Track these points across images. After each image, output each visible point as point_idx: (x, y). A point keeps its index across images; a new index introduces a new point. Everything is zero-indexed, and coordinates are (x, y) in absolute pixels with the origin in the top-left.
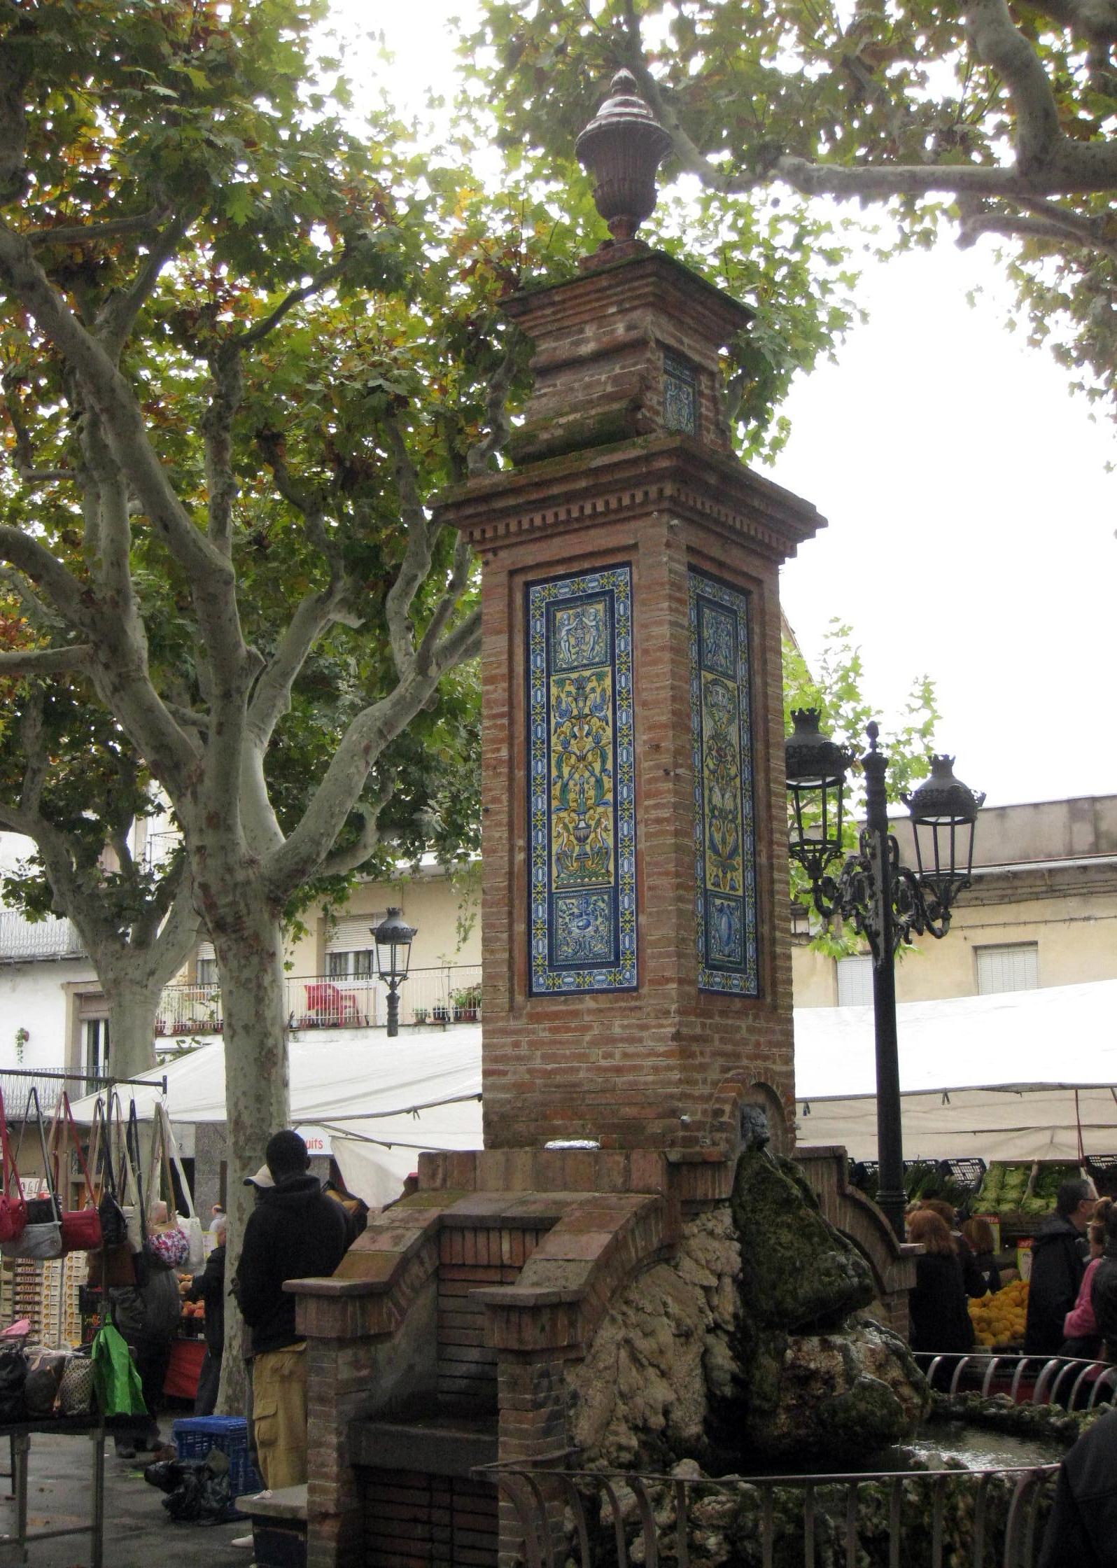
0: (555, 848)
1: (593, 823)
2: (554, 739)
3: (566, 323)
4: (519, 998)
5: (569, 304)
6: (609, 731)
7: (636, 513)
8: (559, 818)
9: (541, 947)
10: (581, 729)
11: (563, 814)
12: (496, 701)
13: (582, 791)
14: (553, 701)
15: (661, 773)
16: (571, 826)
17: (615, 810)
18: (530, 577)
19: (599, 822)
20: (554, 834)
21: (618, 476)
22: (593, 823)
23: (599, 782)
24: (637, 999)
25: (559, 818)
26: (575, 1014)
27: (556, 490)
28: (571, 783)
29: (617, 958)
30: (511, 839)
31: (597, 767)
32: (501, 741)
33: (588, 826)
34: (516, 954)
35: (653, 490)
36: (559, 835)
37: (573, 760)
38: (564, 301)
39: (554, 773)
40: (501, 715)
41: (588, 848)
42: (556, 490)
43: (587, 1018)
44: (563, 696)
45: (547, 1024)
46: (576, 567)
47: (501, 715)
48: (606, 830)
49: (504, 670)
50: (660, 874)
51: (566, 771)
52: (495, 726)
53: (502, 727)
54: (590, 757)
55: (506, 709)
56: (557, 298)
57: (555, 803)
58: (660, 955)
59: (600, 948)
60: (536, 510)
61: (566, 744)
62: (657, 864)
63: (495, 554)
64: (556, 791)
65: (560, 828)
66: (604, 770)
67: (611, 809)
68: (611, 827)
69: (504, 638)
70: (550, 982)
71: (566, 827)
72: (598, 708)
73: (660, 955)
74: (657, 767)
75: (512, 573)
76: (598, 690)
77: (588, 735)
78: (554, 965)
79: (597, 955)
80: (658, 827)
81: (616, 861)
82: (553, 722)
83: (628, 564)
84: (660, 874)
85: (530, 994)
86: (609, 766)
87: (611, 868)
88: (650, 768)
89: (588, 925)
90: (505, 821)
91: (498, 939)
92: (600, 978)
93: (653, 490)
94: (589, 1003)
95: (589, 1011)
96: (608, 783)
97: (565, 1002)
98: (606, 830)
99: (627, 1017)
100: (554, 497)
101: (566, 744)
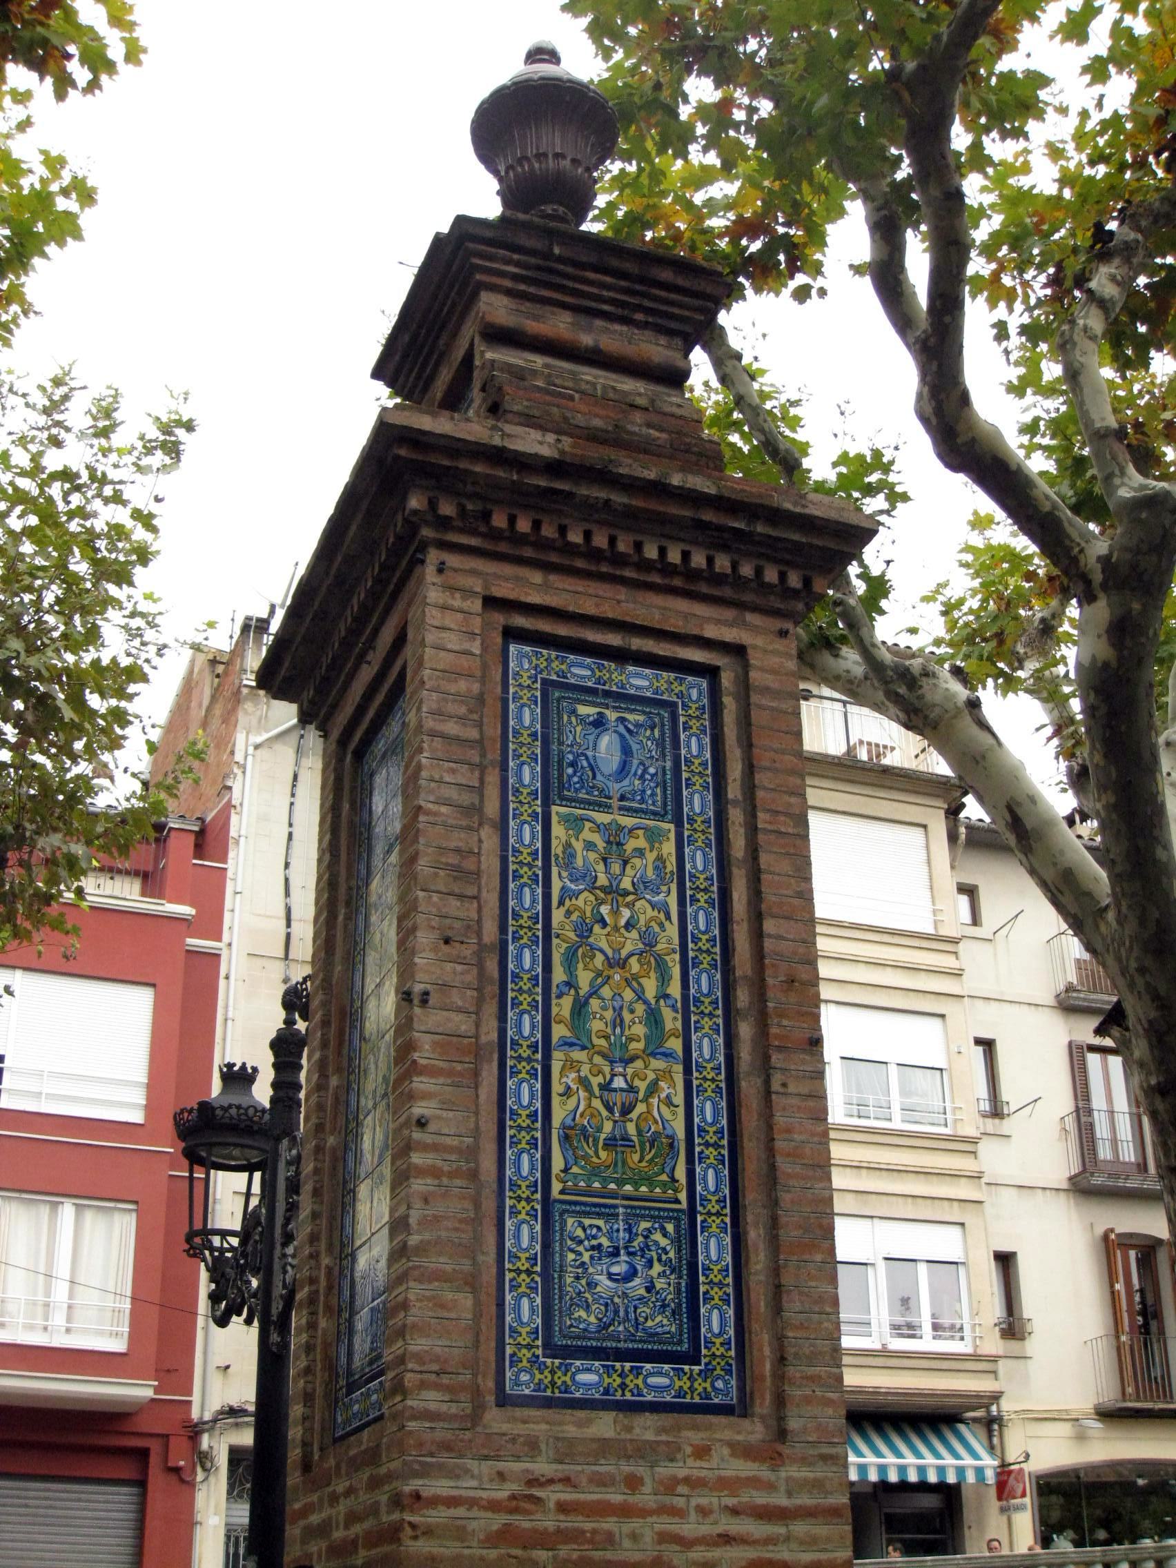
2: (557, 916)
13: (618, 1022)
18: (520, 621)
23: (653, 1017)
25: (571, 1065)
31: (650, 987)
39: (559, 975)
61: (584, 931)
64: (563, 1007)
86: (675, 989)
92: (658, 1380)
96: (671, 1020)
101: (584, 931)
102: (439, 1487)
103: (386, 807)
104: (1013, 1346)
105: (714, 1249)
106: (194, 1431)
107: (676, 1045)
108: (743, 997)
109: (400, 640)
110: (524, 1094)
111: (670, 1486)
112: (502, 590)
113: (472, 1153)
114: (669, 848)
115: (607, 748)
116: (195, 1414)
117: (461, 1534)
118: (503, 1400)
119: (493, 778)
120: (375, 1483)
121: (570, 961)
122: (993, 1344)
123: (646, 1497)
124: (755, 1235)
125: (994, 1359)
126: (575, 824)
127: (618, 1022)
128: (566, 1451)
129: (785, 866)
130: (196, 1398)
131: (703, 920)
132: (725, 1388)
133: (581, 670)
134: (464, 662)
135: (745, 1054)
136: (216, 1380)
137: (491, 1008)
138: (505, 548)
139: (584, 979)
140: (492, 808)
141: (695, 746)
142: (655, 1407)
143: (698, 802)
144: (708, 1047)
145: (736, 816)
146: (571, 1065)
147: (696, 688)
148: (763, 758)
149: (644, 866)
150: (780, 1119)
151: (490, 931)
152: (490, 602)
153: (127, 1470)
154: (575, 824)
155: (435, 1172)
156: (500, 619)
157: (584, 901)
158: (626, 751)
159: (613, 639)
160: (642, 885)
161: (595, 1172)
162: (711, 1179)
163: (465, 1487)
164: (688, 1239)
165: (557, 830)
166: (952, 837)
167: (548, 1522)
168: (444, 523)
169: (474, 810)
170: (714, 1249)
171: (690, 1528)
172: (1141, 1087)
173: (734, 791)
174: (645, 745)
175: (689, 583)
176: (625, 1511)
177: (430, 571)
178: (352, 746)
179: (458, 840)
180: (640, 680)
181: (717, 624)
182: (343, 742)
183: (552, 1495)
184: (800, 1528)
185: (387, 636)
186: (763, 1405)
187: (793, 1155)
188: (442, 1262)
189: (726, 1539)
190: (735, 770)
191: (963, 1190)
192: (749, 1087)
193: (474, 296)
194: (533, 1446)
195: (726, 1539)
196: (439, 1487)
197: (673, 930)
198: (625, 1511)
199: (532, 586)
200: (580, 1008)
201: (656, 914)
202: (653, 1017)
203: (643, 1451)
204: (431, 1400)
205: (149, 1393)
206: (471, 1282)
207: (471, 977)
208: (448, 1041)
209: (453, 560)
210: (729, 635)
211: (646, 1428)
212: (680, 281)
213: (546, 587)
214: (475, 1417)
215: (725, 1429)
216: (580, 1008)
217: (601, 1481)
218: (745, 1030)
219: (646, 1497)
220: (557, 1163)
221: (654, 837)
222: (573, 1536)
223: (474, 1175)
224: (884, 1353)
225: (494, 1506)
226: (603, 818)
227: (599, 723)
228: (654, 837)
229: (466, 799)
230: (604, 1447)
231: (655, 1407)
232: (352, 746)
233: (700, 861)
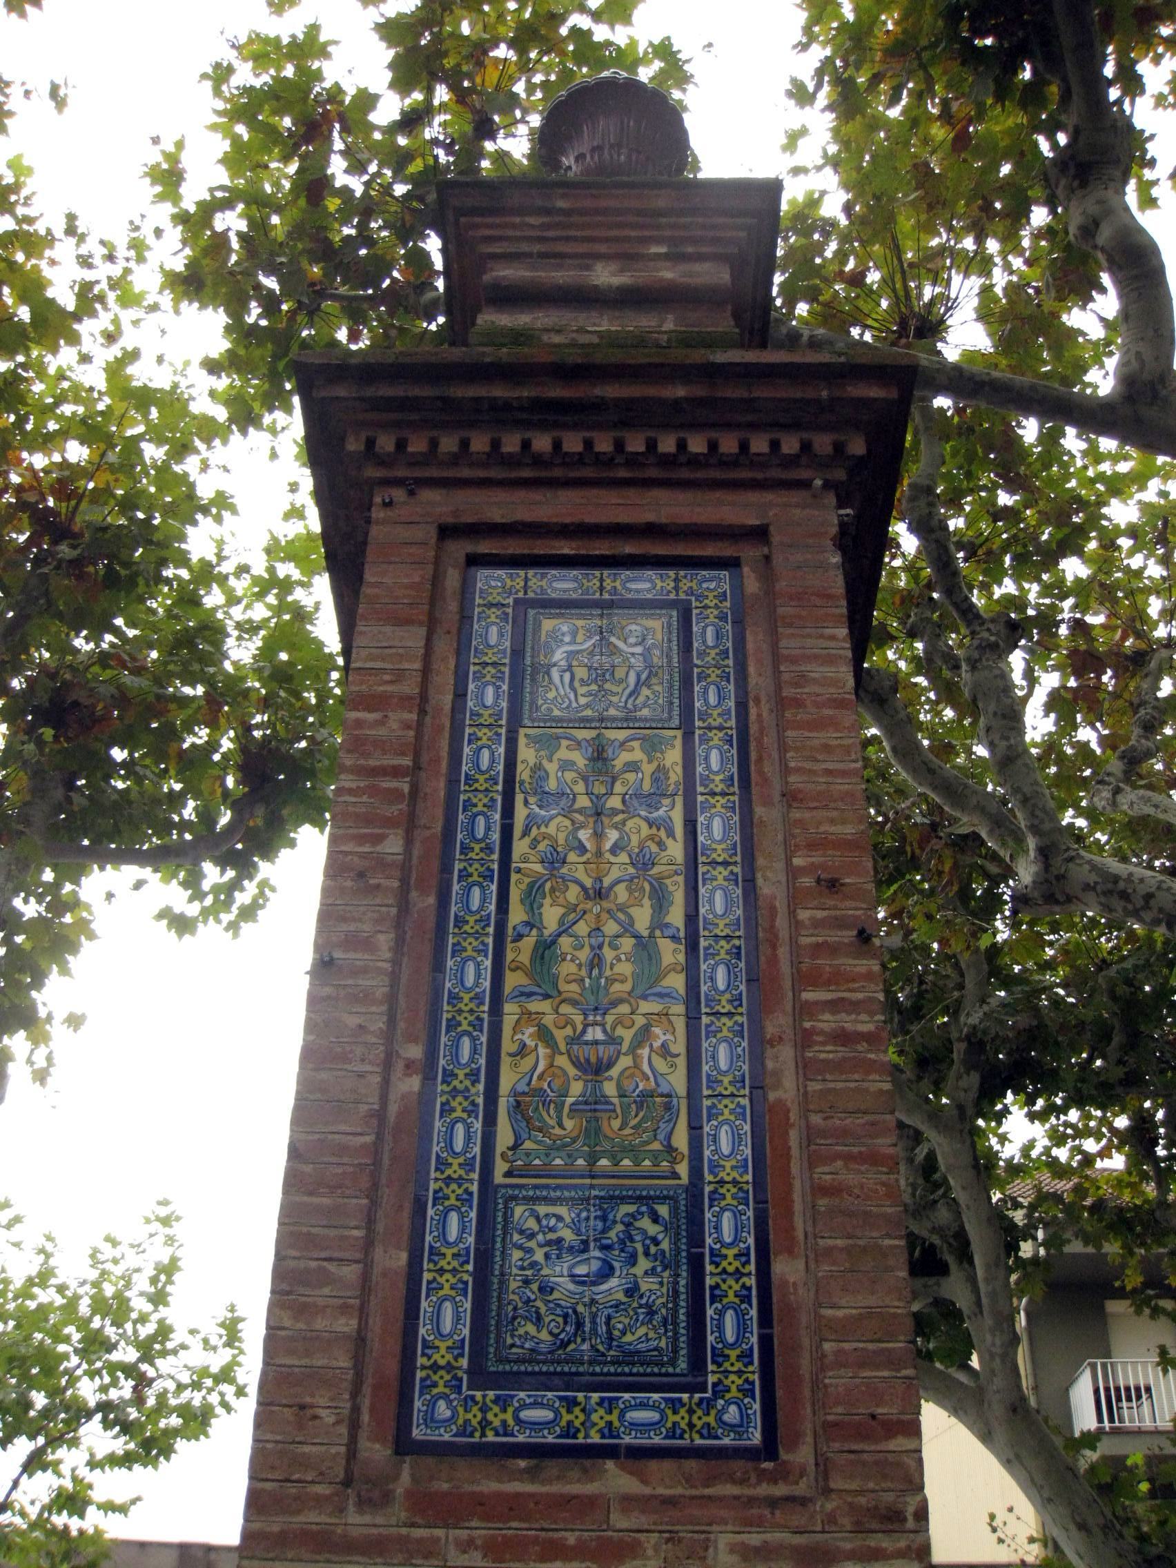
0: (507, 1081)
1: (627, 1035)
2: (520, 847)
3: (561, 248)
4: (375, 1451)
5: (575, 219)
6: (676, 849)
7: (778, 476)
8: (527, 1016)
9: (447, 1318)
10: (598, 836)
11: (535, 1006)
12: (381, 745)
13: (596, 961)
14: (523, 773)
15: (849, 935)
16: (560, 1035)
17: (692, 1019)
18: (484, 547)
19: (644, 1035)
20: (508, 1046)
21: (762, 392)
22: (627, 1035)
23: (645, 946)
24: (773, 1478)
25: (527, 1016)
26: (587, 1505)
27: (610, 391)
28: (565, 942)
29: (697, 1365)
30: (389, 1035)
31: (642, 917)
32: (389, 822)
33: (613, 1040)
34: (375, 1323)
35: (823, 443)
36: (522, 1051)
37: (573, 893)
38: (568, 213)
39: (517, 915)
40: (396, 772)
41: (610, 1089)
42: (610, 391)
43: (619, 1521)
44: (552, 768)
45: (479, 1530)
46: (601, 548)
47: (396, 772)
48: (665, 1051)
49: (410, 687)
50: (848, 1158)
51: (551, 916)
52: (373, 791)
53: (396, 795)
54: (621, 893)
55: (407, 761)
56: (561, 204)
57: (512, 980)
58: (865, 1360)
59: (640, 1336)
60: (543, 426)
61: (554, 861)
62: (843, 1134)
63: (412, 493)
64: (521, 952)
65: (528, 1035)
66: (659, 924)
67: (679, 1009)
68: (679, 1047)
69: (414, 638)
70: (474, 1416)
71: (544, 1035)
72: (652, 799)
73: (865, 1360)
74: (840, 923)
75: (447, 532)
76: (648, 769)
77: (614, 850)
78: (488, 1368)
79: (630, 1356)
80: (842, 1052)
81: (695, 1128)
82: (520, 813)
83: (731, 564)
84: (848, 1158)
85: (404, 1446)
86: (676, 916)
87: (681, 1140)
88: (816, 924)
89: (607, 1271)
90: (380, 992)
91: (325, 1278)
92: (642, 1415)
93: (823, 443)
94: (616, 1479)
95: (629, 1502)
96: (671, 953)
97: (532, 1474)
98: (665, 1051)
99: (759, 1523)
100: (599, 406)
107: (677, 982)
114: (673, 756)
157: (558, 827)
200: (545, 949)
202: (645, 946)
220: (504, 1136)
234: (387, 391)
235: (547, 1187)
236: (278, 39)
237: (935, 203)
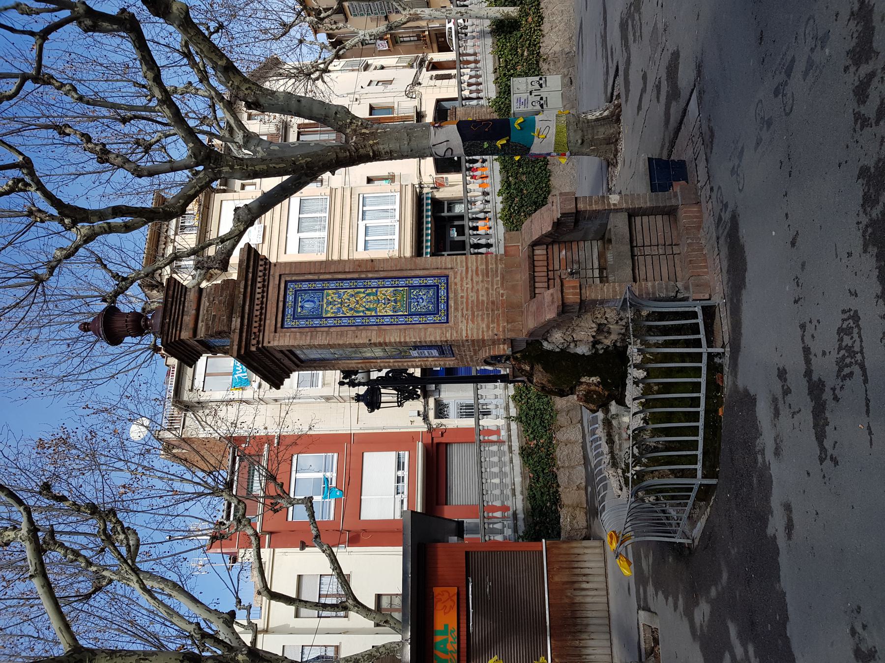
2: (348, 315)
13: (370, 302)
18: (279, 325)
23: (368, 295)
25: (380, 311)
31: (362, 295)
39: (361, 314)
57: (373, 314)
61: (351, 309)
64: (368, 313)
86: (362, 290)
92: (442, 293)
96: (369, 291)
101: (351, 309)
102: (464, 334)
103: (314, 355)
104: (397, 179)
105: (416, 282)
106: (430, 429)
107: (374, 290)
108: (363, 276)
109: (282, 352)
110: (387, 320)
111: (462, 290)
112: (273, 328)
113: (400, 330)
114: (330, 291)
115: (307, 305)
116: (426, 430)
117: (472, 329)
118: (447, 322)
119: (318, 329)
120: (463, 346)
121: (357, 312)
122: (396, 186)
123: (465, 294)
124: (413, 273)
125: (401, 186)
126: (327, 312)
127: (370, 302)
128: (456, 309)
129: (333, 266)
130: (420, 430)
131: (346, 284)
132: (443, 279)
133: (290, 311)
134: (292, 336)
135: (376, 276)
136: (415, 424)
137: (370, 327)
138: (262, 328)
139: (362, 309)
140: (326, 329)
141: (305, 286)
142: (447, 293)
143: (319, 285)
144: (374, 283)
145: (322, 277)
146: (380, 311)
147: (291, 286)
148: (307, 271)
149: (335, 297)
150: (389, 268)
151: (353, 328)
152: (275, 332)
153: (442, 448)
154: (327, 312)
155: (405, 337)
156: (279, 330)
157: (344, 309)
158: (308, 301)
159: (281, 304)
160: (339, 297)
161: (402, 306)
162: (402, 283)
163: (464, 328)
164: (414, 287)
165: (329, 315)
166: (224, 191)
167: (470, 313)
168: (258, 342)
169: (327, 332)
170: (416, 282)
171: (470, 286)
172: (531, 334)
173: (316, 277)
174: (306, 297)
175: (265, 287)
176: (467, 299)
177: (271, 345)
178: (298, 363)
179: (334, 335)
180: (290, 298)
181: (273, 283)
182: (298, 366)
183: (465, 312)
184: (470, 265)
185: (279, 356)
186: (446, 272)
187: (396, 266)
188: (422, 334)
189: (472, 280)
190: (310, 277)
191: (347, 193)
192: (382, 274)
193: (182, 341)
194: (456, 316)
195: (472, 280)
196: (464, 334)
197: (349, 291)
198: (467, 299)
199: (270, 323)
200: (368, 309)
201: (346, 294)
202: (368, 295)
203: (456, 296)
204: (448, 335)
205: (420, 443)
206: (426, 329)
207: (364, 332)
208: (379, 336)
209: (266, 340)
210: (277, 278)
211: (451, 295)
212: (172, 288)
213: (270, 319)
214: (451, 327)
215: (451, 279)
216: (368, 309)
217: (462, 303)
218: (370, 275)
219: (465, 294)
220: (401, 313)
221: (328, 295)
222: (472, 308)
223: (405, 329)
224: (400, 221)
225: (467, 323)
226: (325, 306)
227: (302, 307)
228: (328, 295)
229: (325, 334)
230: (456, 303)
231: (447, 293)
232: (298, 363)
233: (332, 285)
234: (631, 37)
235: (666, 344)
236: (872, 21)
237: (551, 392)
